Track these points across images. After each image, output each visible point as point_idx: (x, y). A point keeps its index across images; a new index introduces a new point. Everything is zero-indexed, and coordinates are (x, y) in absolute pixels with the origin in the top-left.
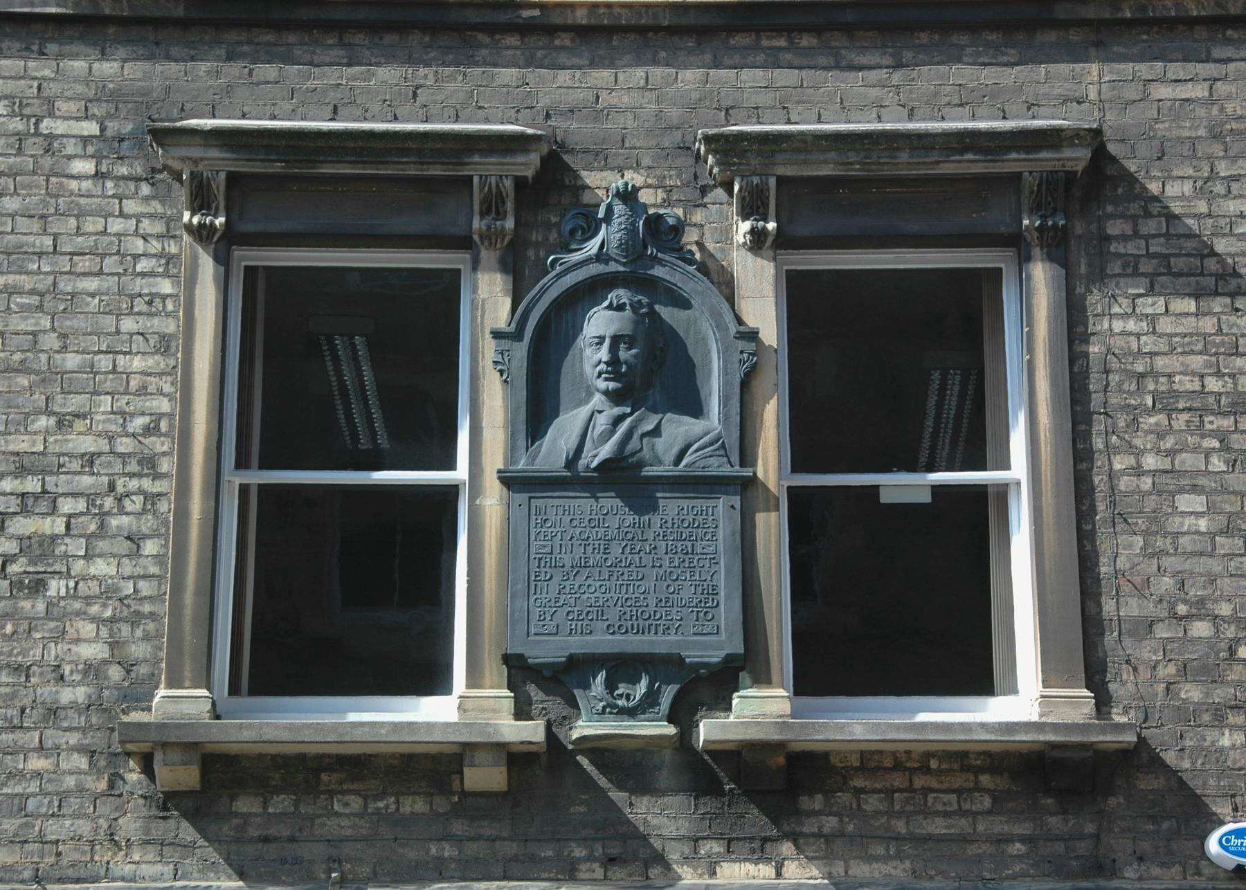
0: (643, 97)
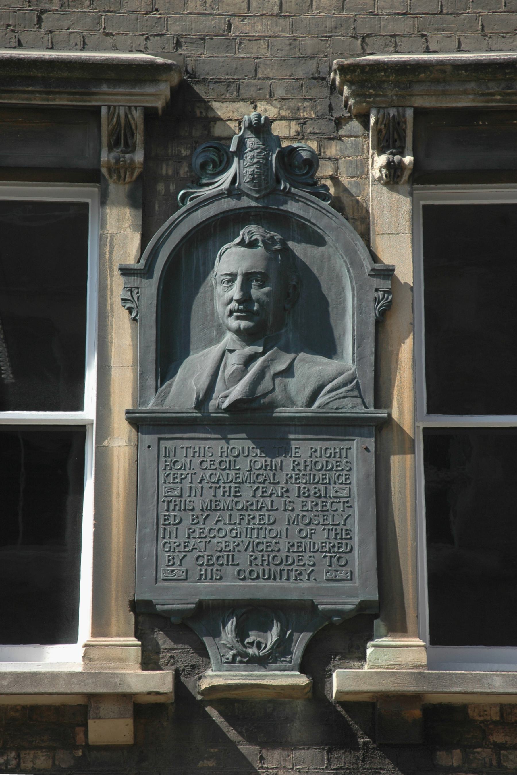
0: (277, 25)
